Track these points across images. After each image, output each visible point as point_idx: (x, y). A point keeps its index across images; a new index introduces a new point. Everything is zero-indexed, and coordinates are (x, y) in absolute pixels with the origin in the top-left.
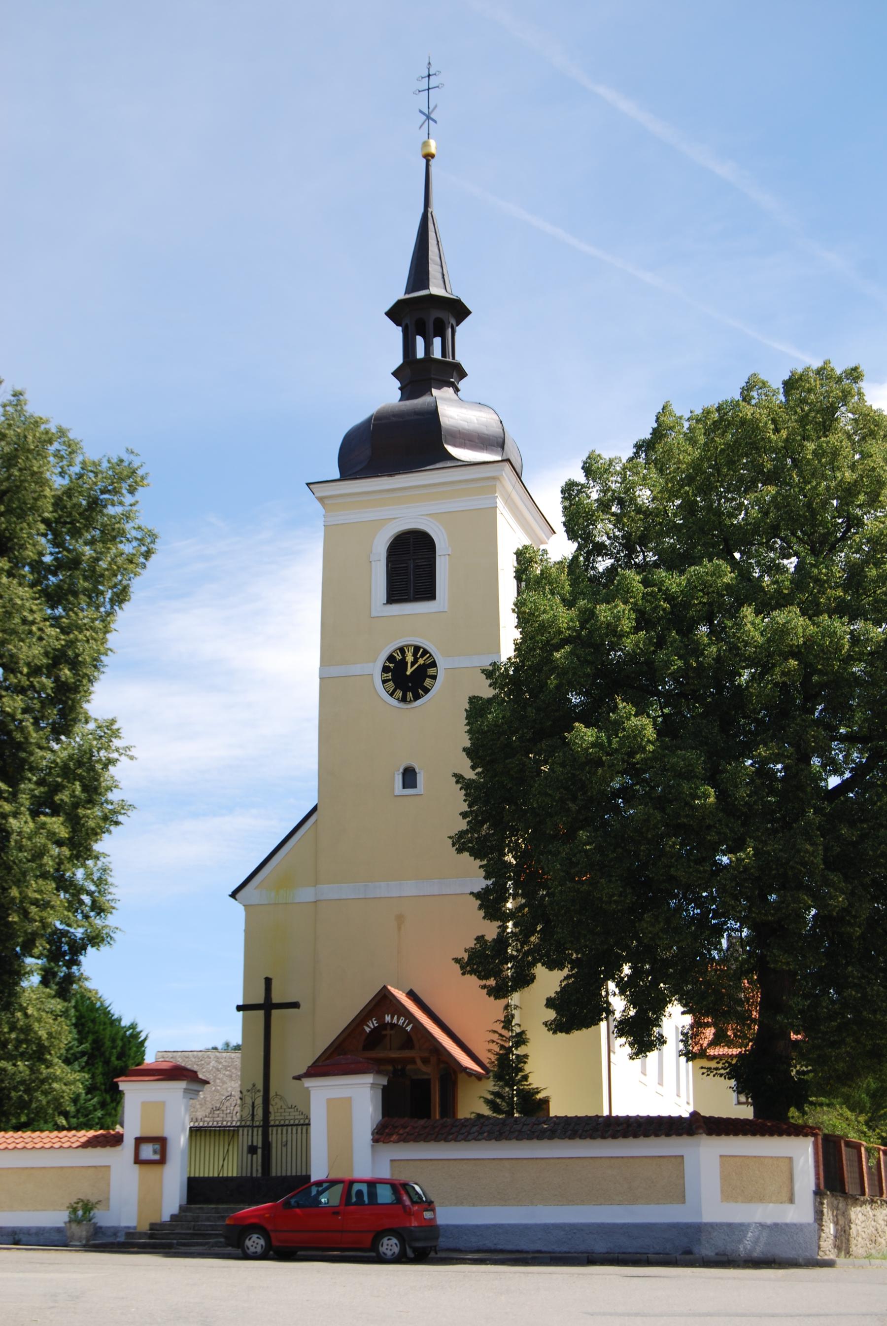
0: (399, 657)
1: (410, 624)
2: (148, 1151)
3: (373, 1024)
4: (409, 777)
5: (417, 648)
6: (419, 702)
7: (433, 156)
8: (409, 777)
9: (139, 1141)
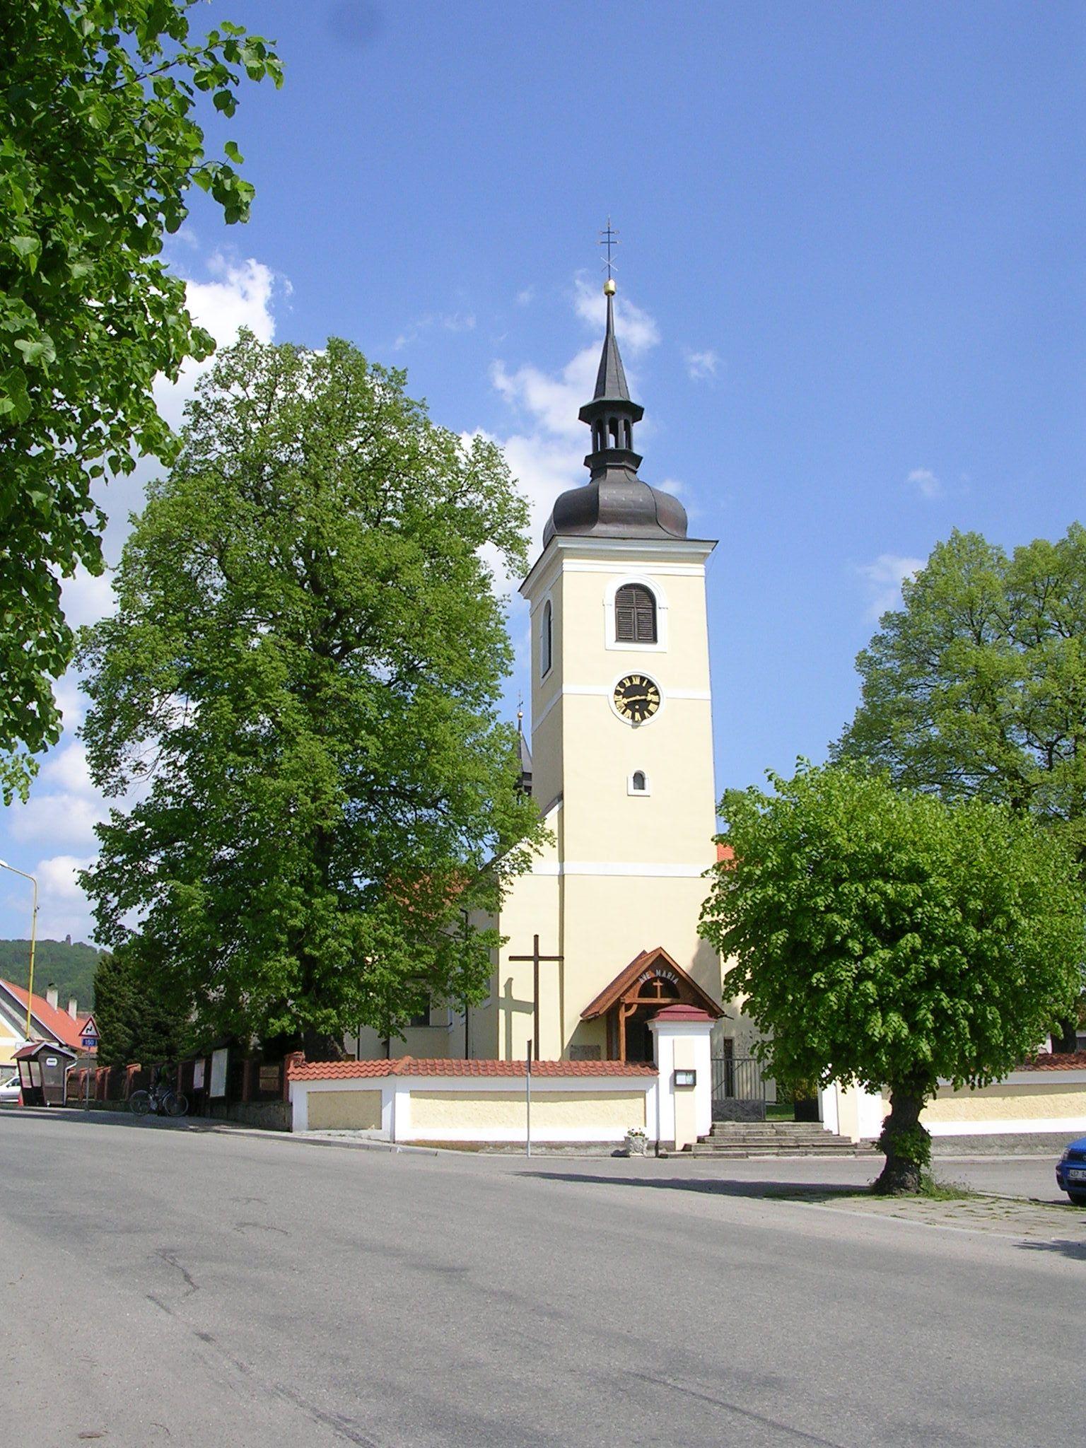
0: (628, 684)
1: (638, 659)
2: (681, 1079)
3: (647, 976)
4: (639, 779)
5: (643, 679)
6: (645, 722)
7: (613, 293)
8: (639, 779)
9: (676, 1072)
